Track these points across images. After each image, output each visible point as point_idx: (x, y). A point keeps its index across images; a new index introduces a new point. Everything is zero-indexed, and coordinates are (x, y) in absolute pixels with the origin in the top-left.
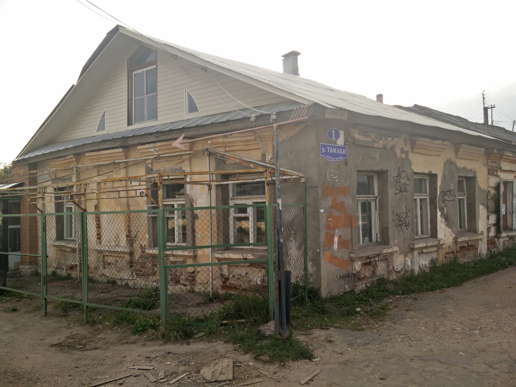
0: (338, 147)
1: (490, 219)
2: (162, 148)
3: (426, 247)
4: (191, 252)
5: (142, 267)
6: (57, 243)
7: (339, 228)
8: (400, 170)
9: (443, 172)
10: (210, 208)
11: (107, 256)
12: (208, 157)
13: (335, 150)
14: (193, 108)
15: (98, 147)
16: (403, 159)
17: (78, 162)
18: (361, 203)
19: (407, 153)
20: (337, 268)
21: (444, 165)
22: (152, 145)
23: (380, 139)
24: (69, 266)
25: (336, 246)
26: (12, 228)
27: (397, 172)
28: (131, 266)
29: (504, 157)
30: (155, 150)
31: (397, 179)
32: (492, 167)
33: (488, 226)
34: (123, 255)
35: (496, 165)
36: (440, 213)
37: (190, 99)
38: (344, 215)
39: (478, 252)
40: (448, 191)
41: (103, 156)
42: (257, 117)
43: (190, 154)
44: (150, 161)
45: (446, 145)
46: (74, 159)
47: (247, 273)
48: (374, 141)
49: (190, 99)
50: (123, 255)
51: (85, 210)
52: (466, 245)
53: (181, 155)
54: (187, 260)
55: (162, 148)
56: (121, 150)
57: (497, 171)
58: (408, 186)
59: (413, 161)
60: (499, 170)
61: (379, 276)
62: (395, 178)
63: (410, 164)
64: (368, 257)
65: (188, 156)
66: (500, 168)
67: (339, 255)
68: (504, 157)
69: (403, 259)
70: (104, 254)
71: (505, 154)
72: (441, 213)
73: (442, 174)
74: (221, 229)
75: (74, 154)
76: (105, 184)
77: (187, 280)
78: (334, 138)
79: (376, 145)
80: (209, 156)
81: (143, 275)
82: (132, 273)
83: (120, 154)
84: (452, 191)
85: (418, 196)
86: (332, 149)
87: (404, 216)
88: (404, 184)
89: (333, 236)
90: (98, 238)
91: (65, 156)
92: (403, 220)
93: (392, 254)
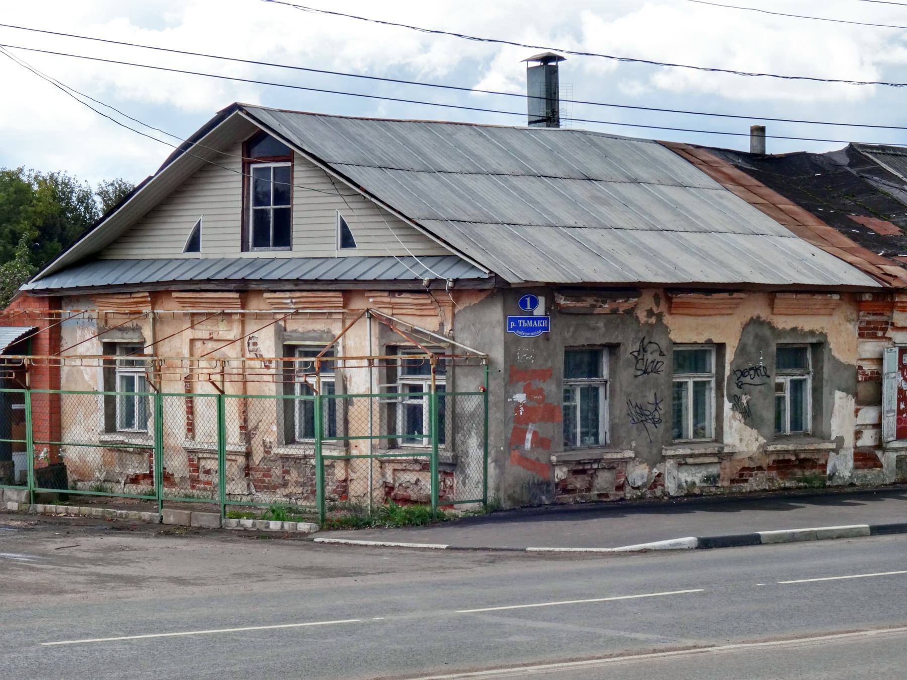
0: (537, 319)
1: (859, 416)
2: (302, 300)
3: (691, 456)
4: (343, 451)
5: (264, 475)
6: (107, 438)
7: (534, 422)
8: (646, 341)
9: (740, 340)
10: (371, 396)
11: (205, 458)
12: (368, 321)
13: (530, 324)
14: (347, 240)
15: (197, 286)
16: (651, 325)
17: (153, 304)
18: (581, 389)
19: (659, 316)
20: (529, 473)
21: (743, 329)
22: (288, 295)
23: (605, 303)
24: (130, 477)
25: (528, 445)
26: (19, 410)
27: (638, 344)
28: (247, 475)
29: (899, 304)
30: (292, 302)
31: (639, 354)
32: (868, 323)
33: (858, 428)
34: (233, 458)
35: (885, 318)
36: (731, 404)
37: (344, 226)
38: (542, 405)
39: (828, 472)
40: (751, 369)
41: (203, 300)
42: (431, 281)
43: (343, 313)
44: (282, 316)
45: (741, 298)
46: (149, 299)
47: (418, 480)
48: (593, 306)
49: (344, 226)
50: (233, 458)
51: (222, 392)
52: (793, 458)
53: (330, 313)
54: (335, 464)
55: (302, 300)
56: (236, 295)
57: (885, 330)
58: (660, 364)
59: (671, 327)
60: (890, 327)
61: (598, 490)
62: (636, 354)
63: (666, 330)
64: (579, 463)
65: (340, 316)
66: (893, 324)
67: (533, 457)
68: (899, 304)
69: (647, 470)
70: (200, 455)
71: (897, 300)
72: (734, 405)
73: (737, 341)
74: (385, 421)
75: (149, 292)
76: (204, 344)
77: (334, 491)
78: (529, 307)
79: (598, 310)
80: (370, 318)
81: (265, 487)
82: (248, 485)
83: (236, 301)
84: (761, 369)
85: (689, 378)
86: (526, 322)
87: (651, 408)
88: (653, 362)
89: (524, 432)
90: (189, 430)
91: (131, 293)
92: (648, 413)
93: (625, 461)
